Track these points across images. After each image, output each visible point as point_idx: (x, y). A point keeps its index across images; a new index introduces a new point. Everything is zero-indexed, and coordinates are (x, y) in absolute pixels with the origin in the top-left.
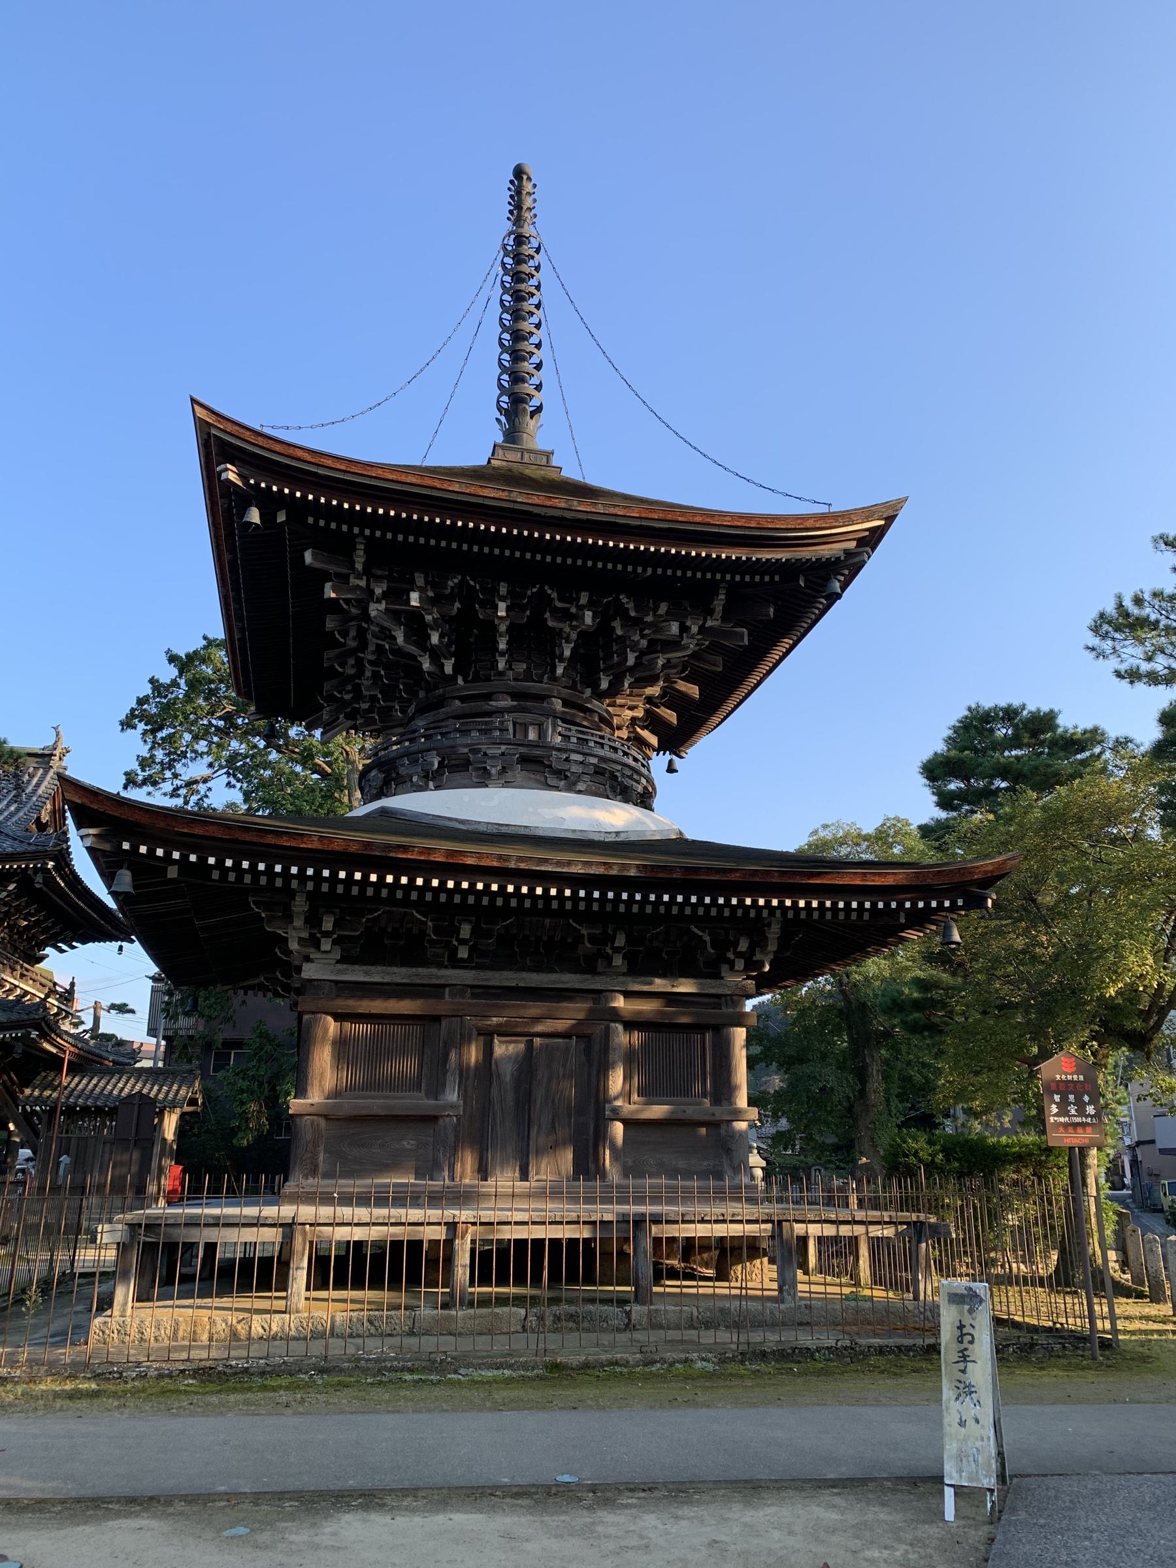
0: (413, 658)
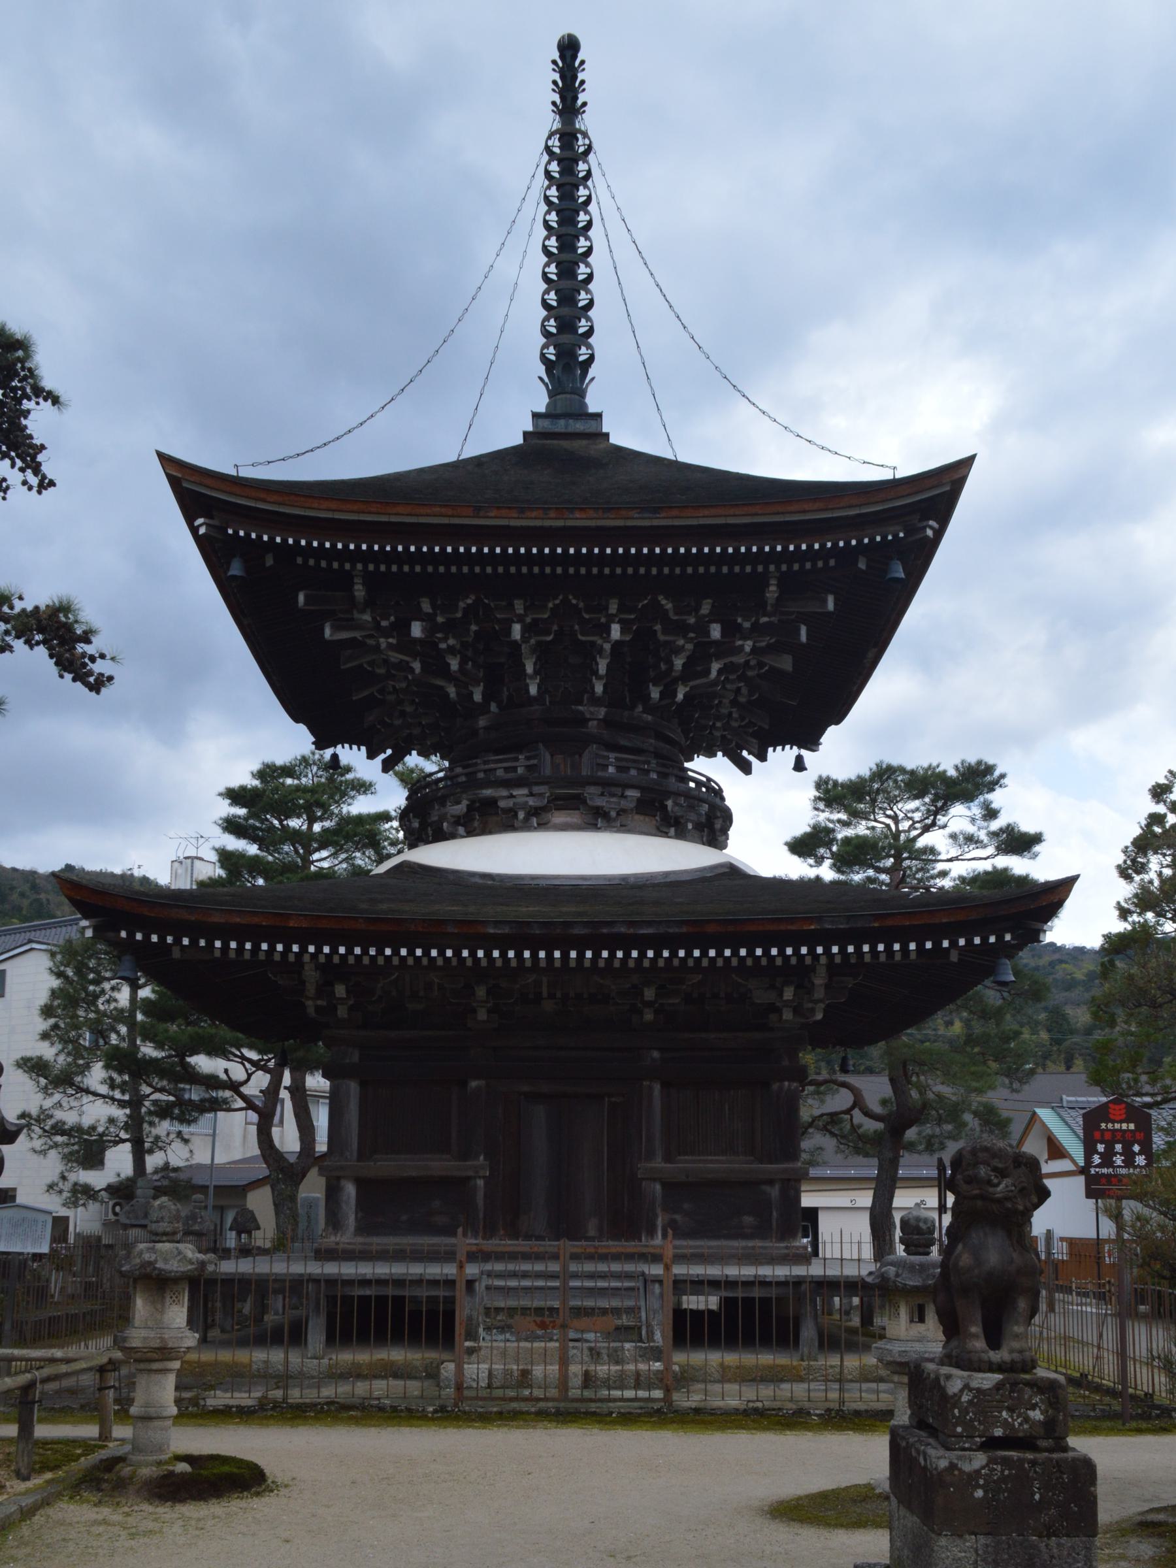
0: (442, 688)
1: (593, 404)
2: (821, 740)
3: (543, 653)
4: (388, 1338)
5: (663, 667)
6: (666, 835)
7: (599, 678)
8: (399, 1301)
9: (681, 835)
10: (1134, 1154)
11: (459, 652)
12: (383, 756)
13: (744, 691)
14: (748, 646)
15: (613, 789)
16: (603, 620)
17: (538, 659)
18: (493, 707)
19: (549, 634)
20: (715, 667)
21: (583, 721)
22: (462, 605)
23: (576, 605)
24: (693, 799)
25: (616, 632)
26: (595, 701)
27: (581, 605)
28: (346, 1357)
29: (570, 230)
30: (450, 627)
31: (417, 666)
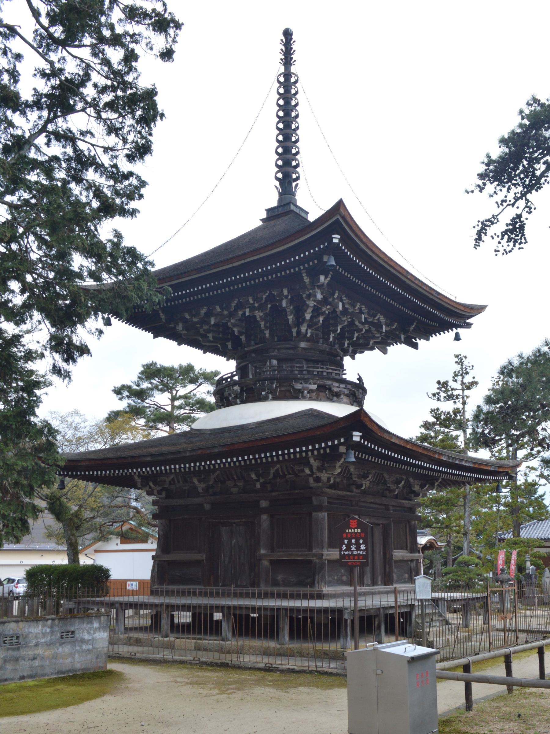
10: (360, 544)
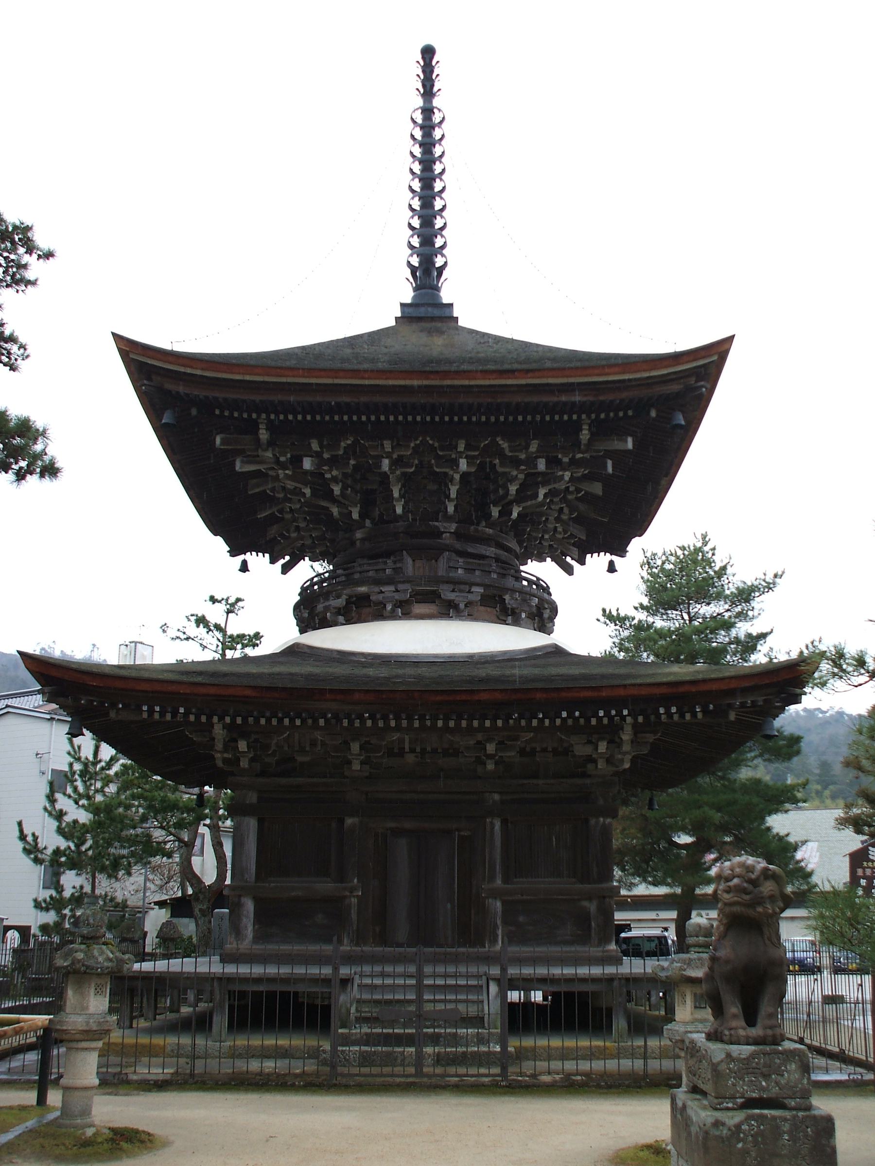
1: (446, 297)
2: (628, 549)
3: (407, 480)
4: (277, 1028)
5: (501, 492)
6: (504, 622)
7: (450, 500)
8: (285, 995)
9: (516, 623)
11: (341, 481)
12: (282, 561)
13: (566, 510)
14: (567, 475)
15: (462, 587)
16: (454, 456)
17: (403, 486)
18: (368, 523)
19: (412, 467)
20: (542, 492)
21: (439, 534)
22: (343, 444)
23: (433, 445)
24: (526, 594)
25: (463, 465)
26: (448, 518)
27: (436, 445)
28: (241, 1041)
29: (430, 212)
30: (334, 462)
31: (307, 491)
